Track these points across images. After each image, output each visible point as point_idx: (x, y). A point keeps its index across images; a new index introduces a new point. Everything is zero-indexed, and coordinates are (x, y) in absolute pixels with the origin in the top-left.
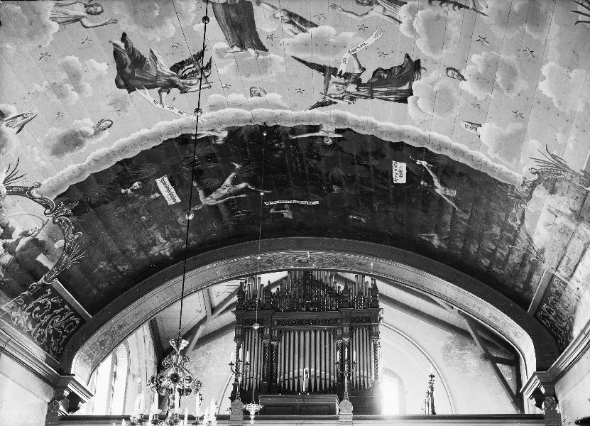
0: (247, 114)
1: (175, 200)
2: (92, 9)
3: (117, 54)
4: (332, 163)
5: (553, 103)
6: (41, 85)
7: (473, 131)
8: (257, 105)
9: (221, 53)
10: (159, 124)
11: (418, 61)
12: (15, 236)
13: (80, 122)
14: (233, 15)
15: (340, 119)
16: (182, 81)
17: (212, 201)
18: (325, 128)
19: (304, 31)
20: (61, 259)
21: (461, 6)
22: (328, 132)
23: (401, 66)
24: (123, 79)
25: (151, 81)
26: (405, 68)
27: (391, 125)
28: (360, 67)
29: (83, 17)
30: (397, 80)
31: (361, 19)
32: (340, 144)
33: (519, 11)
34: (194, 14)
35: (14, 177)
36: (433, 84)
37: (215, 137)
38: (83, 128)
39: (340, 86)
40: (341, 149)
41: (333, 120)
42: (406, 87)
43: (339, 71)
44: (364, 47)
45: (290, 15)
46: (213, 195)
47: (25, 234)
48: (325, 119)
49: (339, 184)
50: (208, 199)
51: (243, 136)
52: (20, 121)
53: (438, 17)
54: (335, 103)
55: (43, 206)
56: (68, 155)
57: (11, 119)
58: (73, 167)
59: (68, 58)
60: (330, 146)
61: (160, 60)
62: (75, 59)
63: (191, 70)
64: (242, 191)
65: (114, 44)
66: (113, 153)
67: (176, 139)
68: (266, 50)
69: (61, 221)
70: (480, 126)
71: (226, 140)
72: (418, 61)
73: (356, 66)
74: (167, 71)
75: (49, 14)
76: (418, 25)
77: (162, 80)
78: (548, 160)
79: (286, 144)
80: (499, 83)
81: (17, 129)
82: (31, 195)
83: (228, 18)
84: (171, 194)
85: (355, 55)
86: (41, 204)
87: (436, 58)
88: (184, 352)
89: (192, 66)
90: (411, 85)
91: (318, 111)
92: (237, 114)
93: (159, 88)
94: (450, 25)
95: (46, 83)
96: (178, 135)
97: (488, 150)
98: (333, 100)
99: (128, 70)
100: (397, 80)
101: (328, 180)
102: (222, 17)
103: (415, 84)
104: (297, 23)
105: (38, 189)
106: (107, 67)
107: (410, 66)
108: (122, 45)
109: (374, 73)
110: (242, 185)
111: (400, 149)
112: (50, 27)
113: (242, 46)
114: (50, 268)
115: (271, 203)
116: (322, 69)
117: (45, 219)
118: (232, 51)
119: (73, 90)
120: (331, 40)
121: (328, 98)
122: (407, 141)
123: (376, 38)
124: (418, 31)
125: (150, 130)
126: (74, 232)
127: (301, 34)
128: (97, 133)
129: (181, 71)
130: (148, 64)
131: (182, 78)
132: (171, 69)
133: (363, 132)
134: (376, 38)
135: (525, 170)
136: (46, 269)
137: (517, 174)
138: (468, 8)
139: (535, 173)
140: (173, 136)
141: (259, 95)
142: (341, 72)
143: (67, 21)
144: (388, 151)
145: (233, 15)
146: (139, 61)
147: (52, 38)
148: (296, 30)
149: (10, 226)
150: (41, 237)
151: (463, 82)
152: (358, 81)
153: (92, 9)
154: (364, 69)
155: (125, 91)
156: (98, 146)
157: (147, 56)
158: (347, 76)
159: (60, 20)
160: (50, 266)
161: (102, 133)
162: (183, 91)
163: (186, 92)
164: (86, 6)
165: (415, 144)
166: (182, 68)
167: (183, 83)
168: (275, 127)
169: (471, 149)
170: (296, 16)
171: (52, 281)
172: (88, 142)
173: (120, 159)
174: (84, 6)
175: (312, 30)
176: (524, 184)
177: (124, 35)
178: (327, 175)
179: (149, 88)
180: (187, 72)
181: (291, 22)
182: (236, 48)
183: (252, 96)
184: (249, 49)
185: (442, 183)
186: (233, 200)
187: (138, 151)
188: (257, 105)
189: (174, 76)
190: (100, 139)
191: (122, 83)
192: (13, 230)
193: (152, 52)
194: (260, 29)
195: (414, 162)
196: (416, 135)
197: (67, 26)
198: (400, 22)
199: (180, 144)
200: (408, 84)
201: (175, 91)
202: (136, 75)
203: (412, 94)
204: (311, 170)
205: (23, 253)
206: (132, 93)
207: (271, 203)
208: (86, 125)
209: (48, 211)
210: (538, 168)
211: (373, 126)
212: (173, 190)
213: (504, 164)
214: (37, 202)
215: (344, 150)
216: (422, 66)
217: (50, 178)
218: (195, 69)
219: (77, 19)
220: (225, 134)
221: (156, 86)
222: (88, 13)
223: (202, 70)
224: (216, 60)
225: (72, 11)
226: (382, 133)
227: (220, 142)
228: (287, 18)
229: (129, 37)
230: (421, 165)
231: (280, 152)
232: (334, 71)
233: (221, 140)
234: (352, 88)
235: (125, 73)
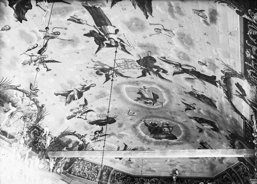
14: (103, 21)
19: (71, 17)
23: (24, 14)
26: (22, 15)
28: (39, 6)
44: (45, 15)
45: (80, 23)
52: (201, 14)
53: (31, 42)
57: (203, 18)
65: (152, 15)
73: (40, 5)
76: (33, 35)
81: (203, 12)
83: (104, 20)
85: (45, 11)
88: (74, 170)
90: (14, 9)
102: (107, 21)
104: (76, 20)
107: (22, 17)
108: (148, 14)
120: (59, 15)
123: (43, 21)
134: (43, 21)
138: (26, 51)
145: (103, 21)
159: (172, 32)
164: (161, 32)
170: (78, 23)
174: (162, 33)
175: (69, 18)
181: (79, 20)
184: (91, 6)
197: (170, 29)
198: (39, 31)
200: (15, 8)
203: (9, 5)
216: (18, 22)
222: (161, 30)
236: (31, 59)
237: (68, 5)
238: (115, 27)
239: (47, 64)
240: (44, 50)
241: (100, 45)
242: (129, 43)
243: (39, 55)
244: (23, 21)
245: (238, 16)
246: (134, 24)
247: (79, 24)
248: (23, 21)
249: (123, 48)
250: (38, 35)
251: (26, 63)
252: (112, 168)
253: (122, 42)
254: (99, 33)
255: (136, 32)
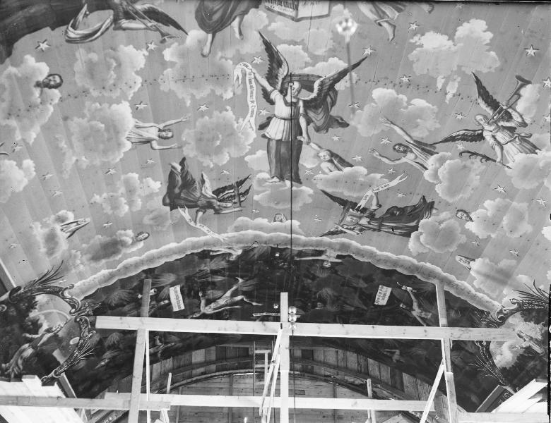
0: (265, 235)
1: (179, 306)
2: (164, 134)
3: (172, 175)
4: (325, 283)
5: (185, 239)
6: (100, 196)
7: (466, 265)
8: (275, 230)
9: (261, 182)
10: (187, 239)
11: (433, 203)
12: (42, 331)
13: (123, 232)
15: (344, 246)
16: (218, 203)
17: (210, 310)
18: (328, 254)
19: (339, 169)
20: (73, 354)
21: (488, 159)
22: (330, 257)
24: (170, 198)
25: (192, 202)
27: (390, 254)
29: (154, 140)
30: (404, 218)
31: (393, 163)
32: (337, 268)
33: (543, 167)
34: (250, 147)
35: (54, 278)
36: (440, 223)
37: (230, 254)
38: (124, 238)
39: (355, 218)
40: (336, 272)
41: (338, 247)
42: (413, 224)
43: (359, 205)
45: (332, 154)
46: (213, 305)
47: (48, 331)
48: (330, 246)
49: (324, 302)
50: (207, 308)
51: (254, 255)
52: (73, 227)
54: (345, 232)
55: (71, 305)
56: (104, 261)
58: (105, 272)
59: (130, 175)
60: (327, 268)
61: (207, 184)
62: (135, 176)
63: (229, 195)
64: (237, 303)
65: (173, 167)
66: (142, 262)
67: (197, 254)
68: (301, 183)
69: (81, 320)
70: (474, 260)
71: (239, 257)
72: (433, 203)
74: (209, 193)
75: (127, 134)
77: (203, 202)
78: (531, 292)
79: (289, 264)
80: (504, 226)
81: (69, 234)
82: (63, 295)
83: (278, 151)
84: (178, 302)
86: (69, 304)
87: (451, 201)
89: (232, 191)
91: (326, 239)
92: (256, 236)
93: (198, 208)
94: (472, 175)
95: (105, 195)
96: (200, 250)
97: (475, 281)
98: (343, 229)
99: (177, 191)
100: (404, 218)
101: (315, 298)
102: (273, 151)
103: (422, 222)
104: (336, 162)
105: (71, 290)
106: (160, 186)
108: (179, 168)
109: (389, 210)
110: (239, 298)
111: (390, 276)
112: (124, 144)
113: (282, 178)
114: (61, 363)
115: (258, 315)
116: (343, 202)
117: (69, 317)
118: (271, 181)
119: (125, 203)
121: (340, 228)
122: (399, 270)
124: (440, 178)
125: (179, 244)
126: (89, 332)
127: (336, 172)
128: (133, 243)
129: (221, 195)
130: (196, 187)
131: (220, 201)
132: (213, 193)
133: (361, 259)
135: (506, 300)
136: (58, 364)
137: (496, 303)
139: (515, 303)
140: (195, 251)
141: (281, 221)
142: (360, 207)
143: (140, 142)
144: (377, 277)
146: (188, 184)
147: (122, 155)
148: (332, 167)
149: (39, 322)
150: (60, 334)
151: (470, 222)
152: (372, 216)
153: (164, 134)
154: (380, 206)
155: (168, 208)
156: (130, 255)
157: (198, 180)
158: (364, 210)
159: (133, 141)
160: (61, 360)
161: (138, 243)
162: (217, 212)
163: (219, 213)
164: (160, 130)
165: (405, 273)
166: (223, 192)
167: (219, 206)
168: (246, 252)
169: (458, 279)
170: (337, 156)
171: (60, 374)
172: (124, 251)
173: (145, 268)
174: (157, 129)
175: (347, 170)
176: (501, 312)
177: (184, 159)
178: (315, 293)
179: (189, 207)
180: (226, 196)
181: (331, 161)
182: (275, 179)
183: (275, 221)
185: (420, 306)
186: (226, 310)
187: (162, 261)
188: (275, 230)
189: (214, 198)
190: (134, 249)
191: (168, 201)
192: (41, 326)
193: (202, 176)
194: (302, 165)
195: (400, 288)
196: (410, 264)
198: (426, 169)
199: (200, 258)
201: (211, 211)
202: (182, 195)
203: (417, 230)
204: (304, 288)
205: (44, 348)
206: (173, 211)
207: (258, 315)
208: (126, 235)
209: (73, 310)
210: (519, 299)
211: (372, 255)
212: (181, 298)
213: (485, 294)
214: (67, 301)
215: (339, 273)
217: (84, 281)
218: (233, 194)
219: (148, 141)
220: (240, 252)
221: (196, 206)
223: (239, 195)
224: (255, 187)
225: (146, 133)
226: (379, 261)
227: (233, 258)
228: (328, 158)
229: (187, 162)
230: (406, 291)
231: (282, 271)
232: (354, 205)
233: (234, 257)
234: (364, 221)
235: (173, 192)
236: (510, 141)
237: (329, 190)
238: (264, 136)
239: (502, 100)
240: (464, 135)
241: (332, 87)
242: (251, 87)
243: (485, 134)
244: (429, 200)
245: (16, 283)
246: (218, 143)
247: (335, 151)
248: (429, 200)
249: (274, 59)
250: (438, 165)
251: (528, 146)
252: (290, 374)
253: (269, 88)
254: (308, 124)
255: (222, 120)
